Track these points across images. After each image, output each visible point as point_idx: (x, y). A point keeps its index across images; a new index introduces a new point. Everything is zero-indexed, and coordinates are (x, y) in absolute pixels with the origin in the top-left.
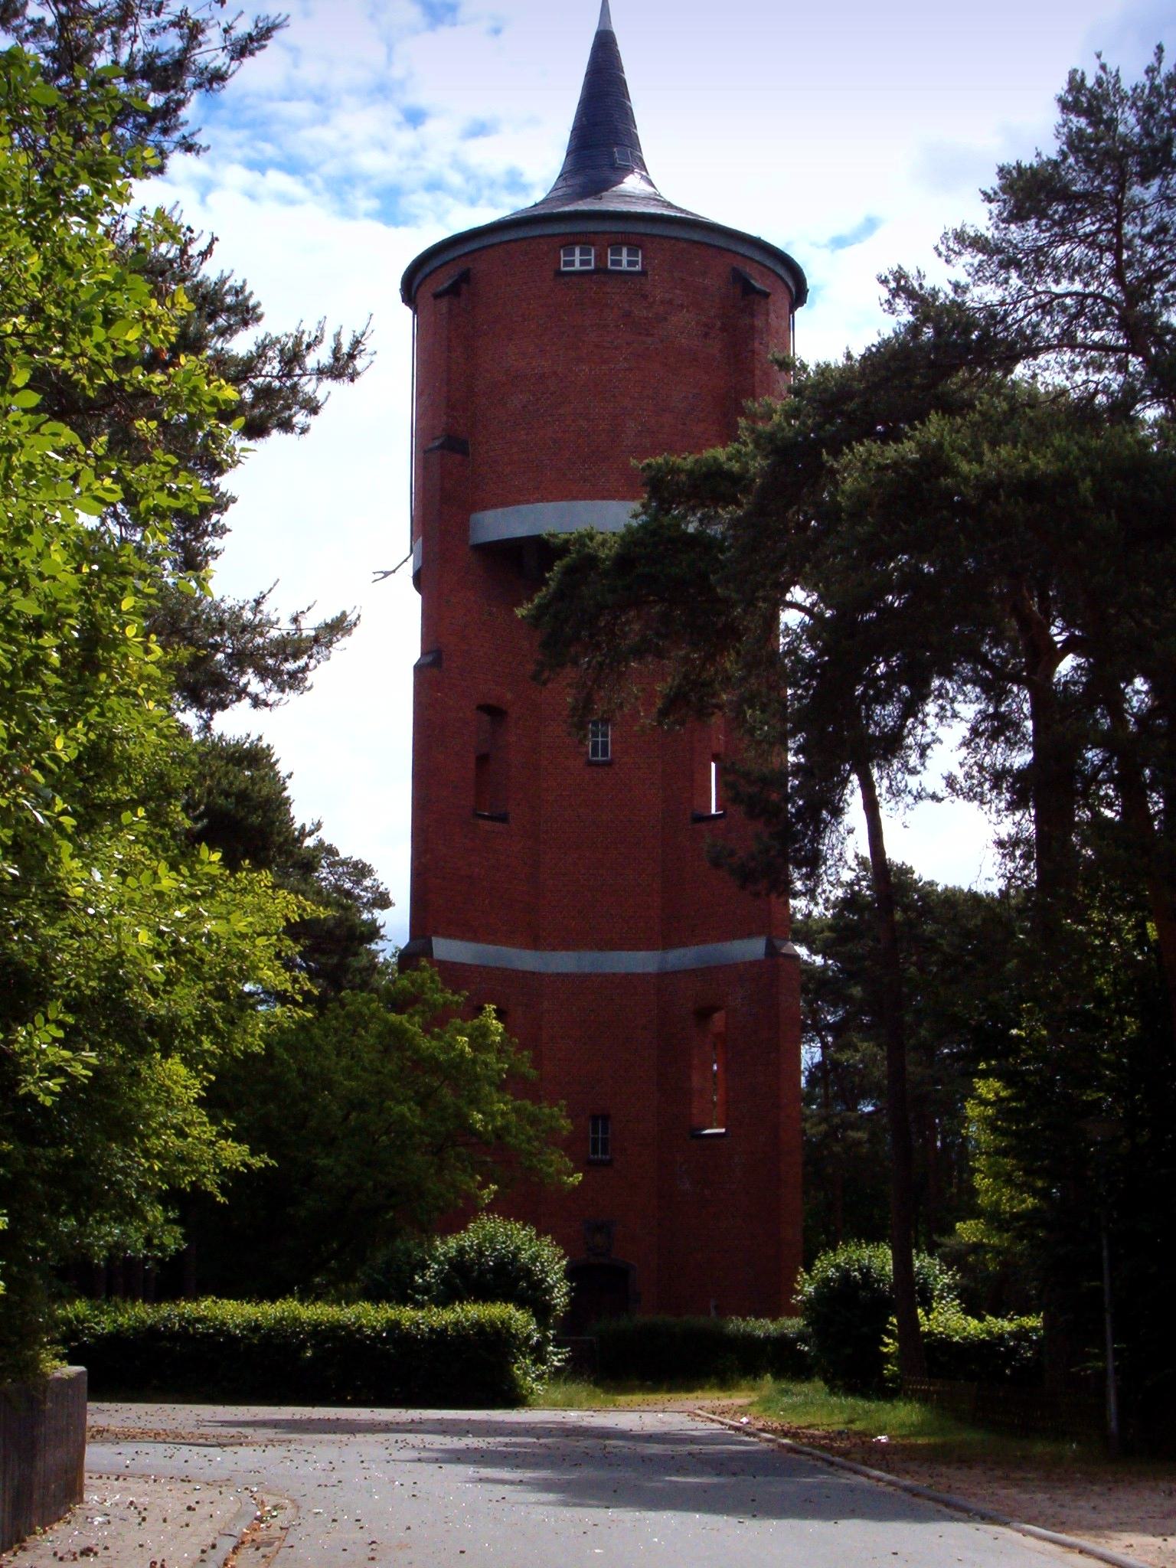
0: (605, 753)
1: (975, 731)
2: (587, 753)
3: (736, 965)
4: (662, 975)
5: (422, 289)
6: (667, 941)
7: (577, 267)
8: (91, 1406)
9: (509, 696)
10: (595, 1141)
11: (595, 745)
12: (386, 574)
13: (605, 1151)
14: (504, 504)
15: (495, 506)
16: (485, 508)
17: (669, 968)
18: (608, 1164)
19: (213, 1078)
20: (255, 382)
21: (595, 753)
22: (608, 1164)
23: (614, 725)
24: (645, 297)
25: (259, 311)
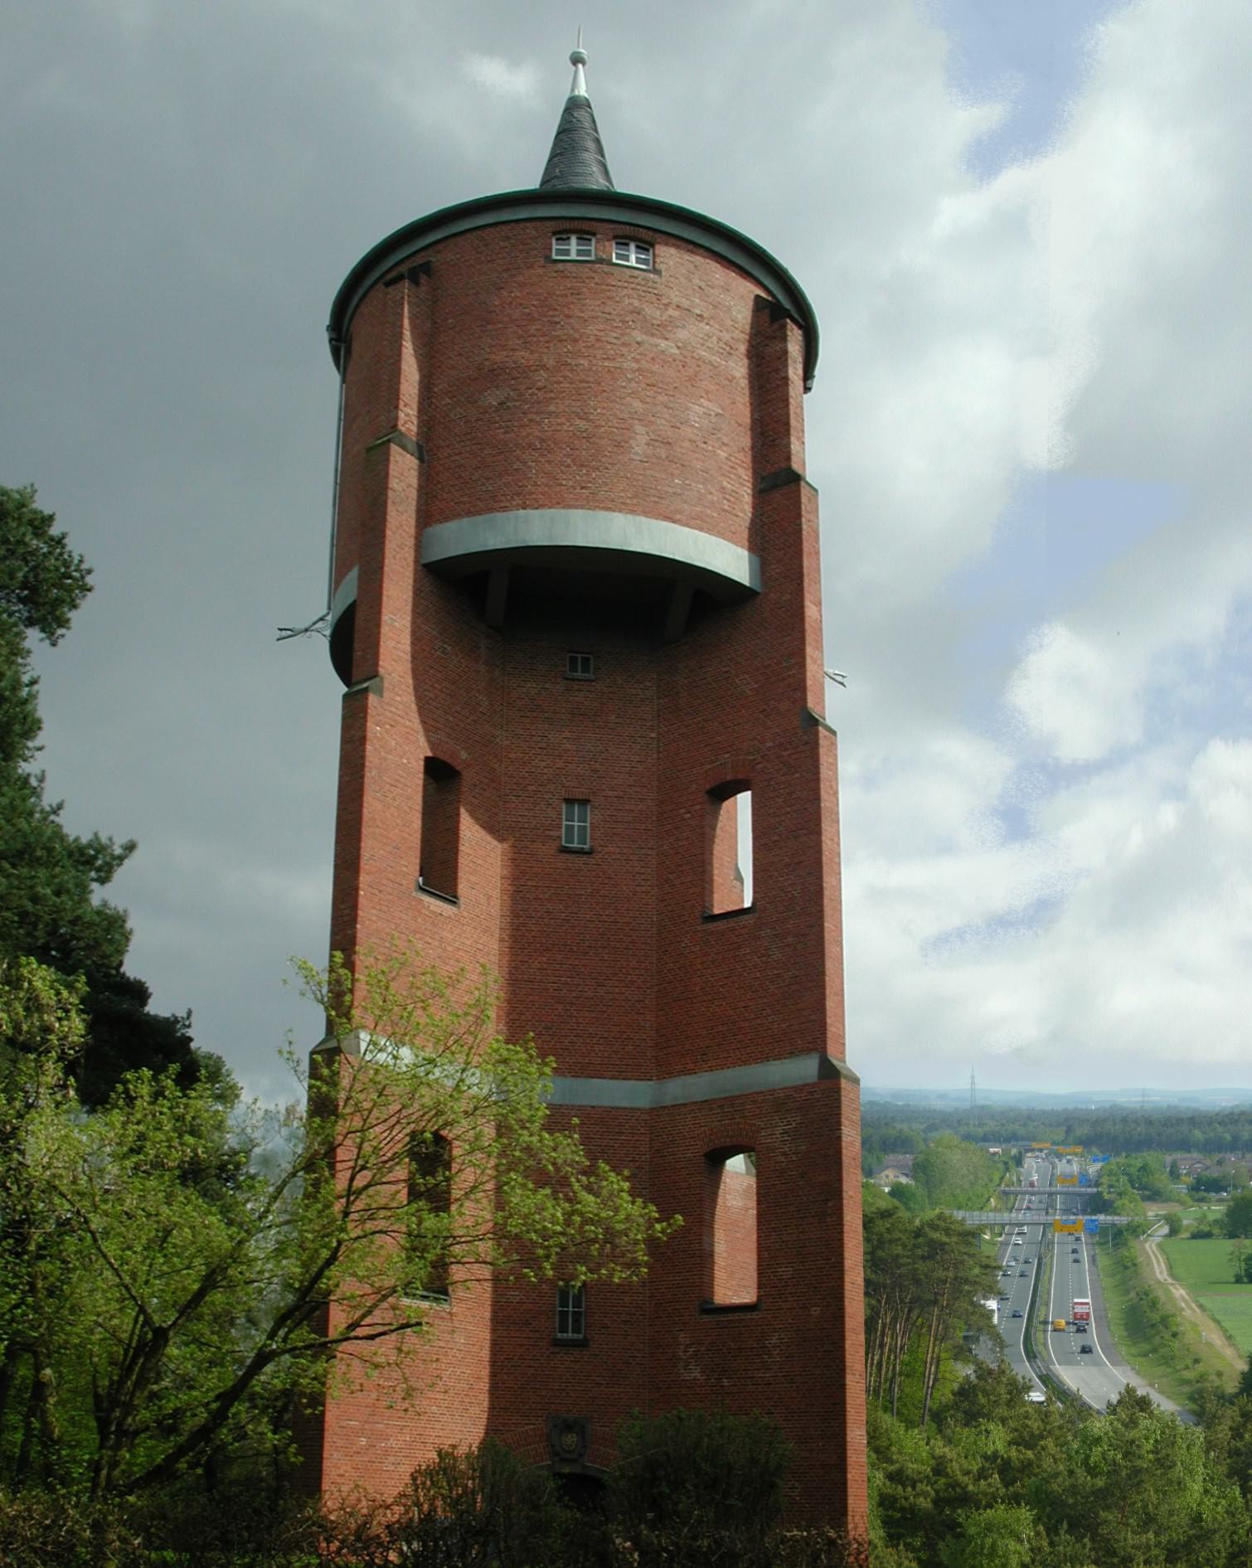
0: (583, 840)
1: (248, 1152)
2: (559, 837)
3: (772, 1092)
4: (656, 1112)
5: (364, 309)
6: (664, 1069)
7: (573, 256)
8: (147, 1009)
9: (464, 755)
10: (564, 1314)
11: (570, 829)
12: (295, 633)
13: (576, 1330)
14: (470, 513)
15: (458, 516)
16: (447, 519)
17: (668, 1102)
18: (583, 1344)
19: (735, 1278)
20: (46, 1017)
21: (570, 839)
22: (583, 1344)
23: (593, 807)
24: (659, 297)
25: (89, 580)
